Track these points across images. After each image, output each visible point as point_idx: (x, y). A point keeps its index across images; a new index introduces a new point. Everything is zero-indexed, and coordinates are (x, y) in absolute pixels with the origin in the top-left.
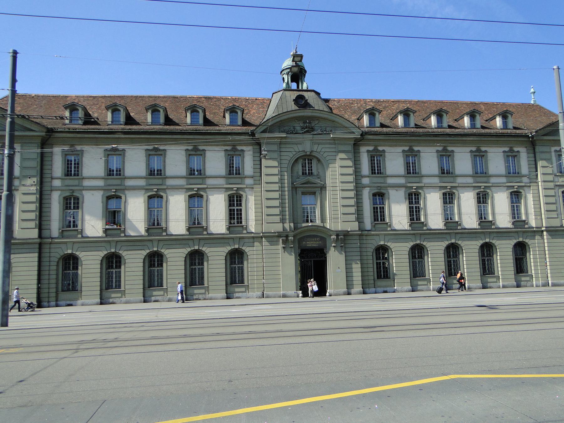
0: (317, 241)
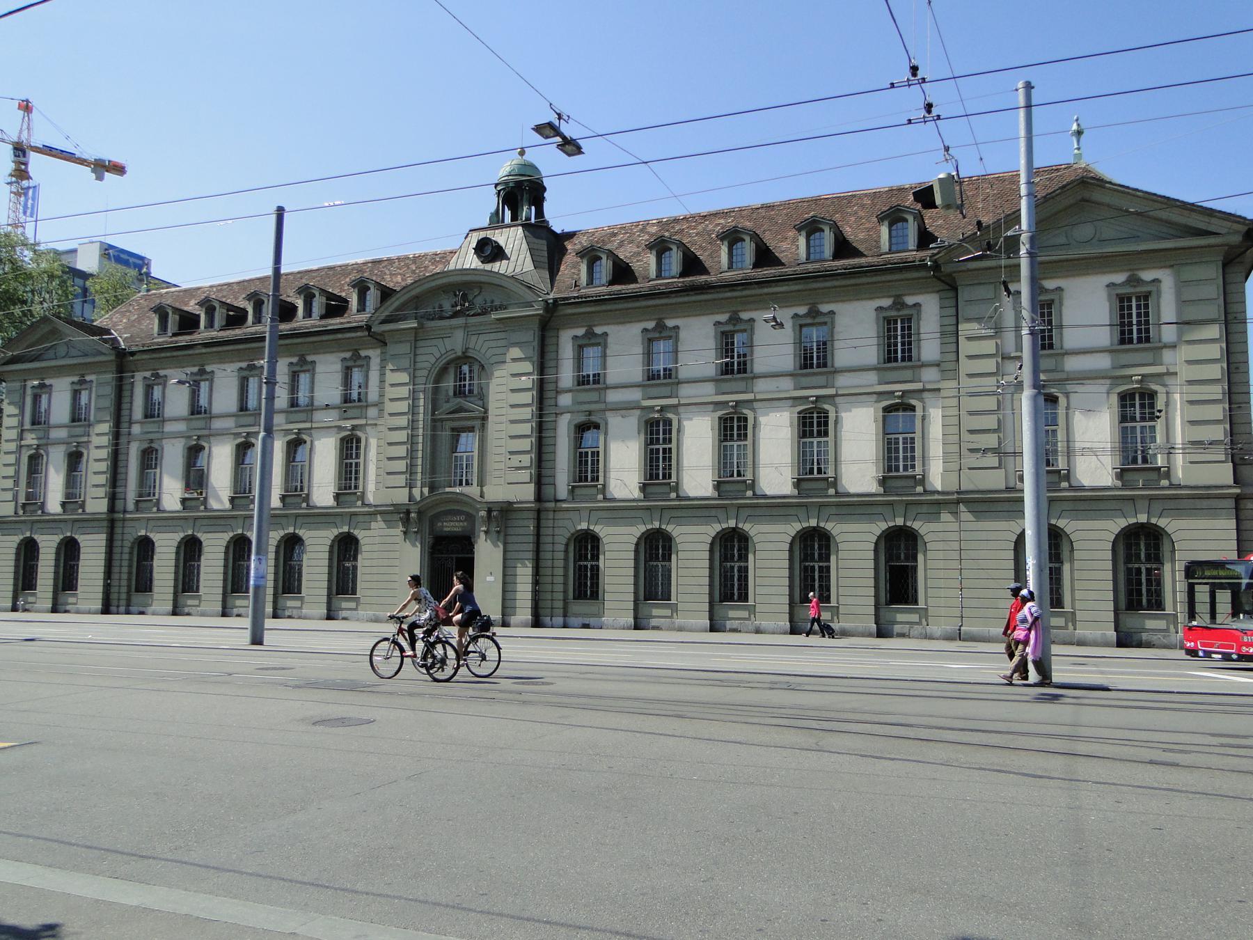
0: (461, 521)
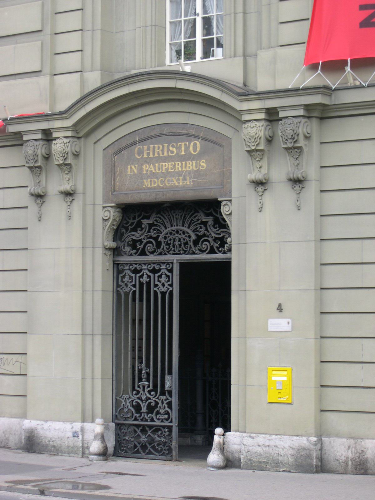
0: (189, 157)
